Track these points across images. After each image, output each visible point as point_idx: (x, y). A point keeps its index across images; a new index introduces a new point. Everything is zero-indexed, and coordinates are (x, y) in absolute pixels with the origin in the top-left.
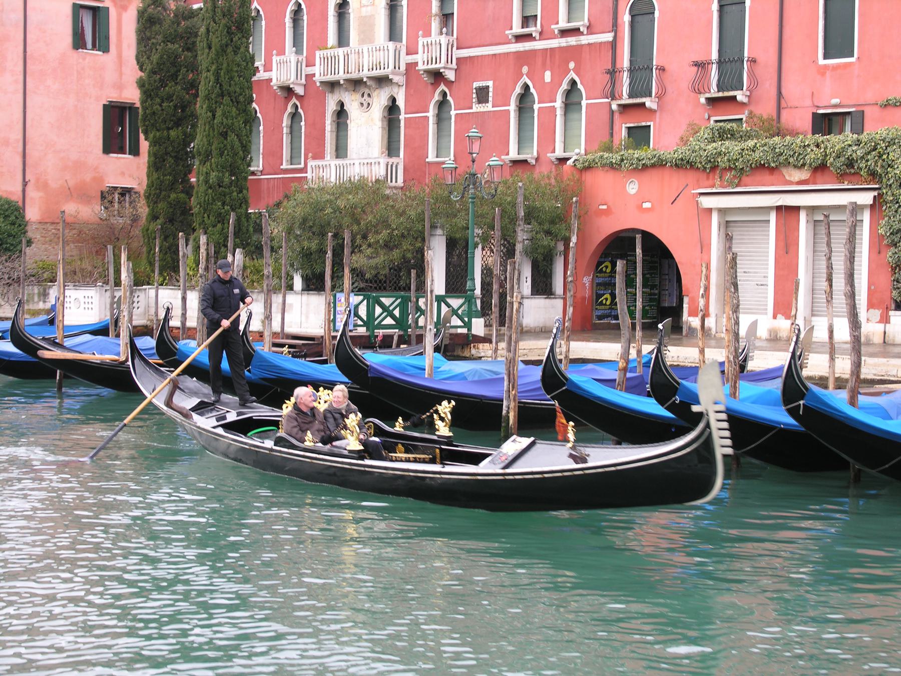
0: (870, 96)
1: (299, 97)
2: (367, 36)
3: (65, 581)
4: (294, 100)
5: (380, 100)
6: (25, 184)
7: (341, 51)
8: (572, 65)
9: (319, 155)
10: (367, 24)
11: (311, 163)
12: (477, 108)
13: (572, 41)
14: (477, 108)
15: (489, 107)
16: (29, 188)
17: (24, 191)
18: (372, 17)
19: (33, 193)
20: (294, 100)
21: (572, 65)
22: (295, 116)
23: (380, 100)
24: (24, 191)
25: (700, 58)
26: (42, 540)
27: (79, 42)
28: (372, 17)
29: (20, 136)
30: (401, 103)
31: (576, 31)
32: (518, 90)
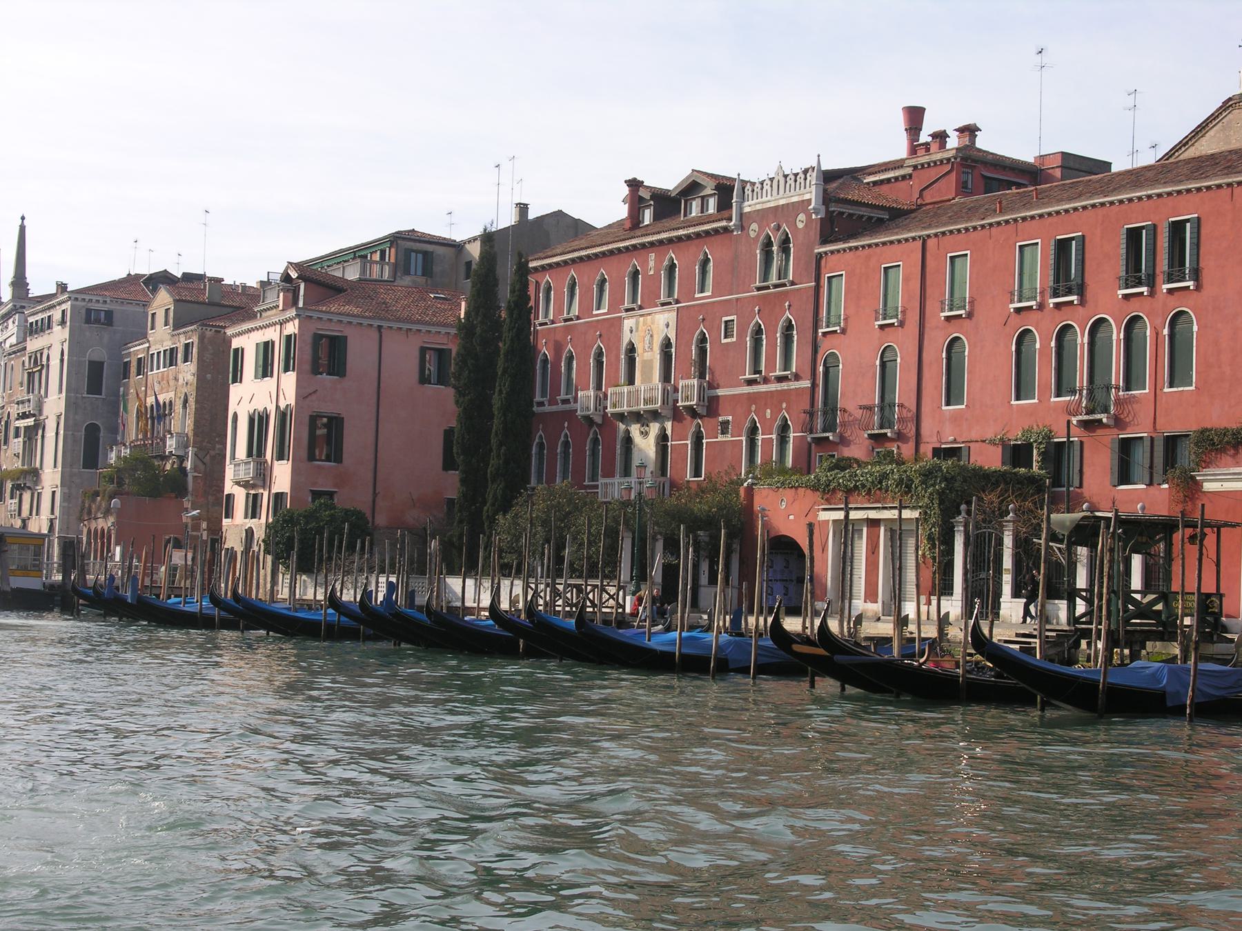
0: (974, 435)
1: (599, 426)
2: (647, 378)
3: (91, 740)
4: (595, 428)
5: (654, 428)
6: (375, 494)
7: (626, 389)
8: (784, 405)
9: (609, 473)
10: (648, 365)
11: (602, 481)
12: (720, 438)
13: (784, 386)
14: (720, 438)
15: (728, 438)
16: (378, 500)
17: (374, 501)
18: (651, 361)
19: (381, 504)
20: (595, 428)
21: (784, 405)
22: (595, 441)
23: (654, 428)
24: (374, 501)
25: (865, 402)
26: (553, 753)
27: (424, 379)
28: (651, 361)
29: (373, 456)
30: (669, 432)
31: (571, 320)
32: (747, 424)
